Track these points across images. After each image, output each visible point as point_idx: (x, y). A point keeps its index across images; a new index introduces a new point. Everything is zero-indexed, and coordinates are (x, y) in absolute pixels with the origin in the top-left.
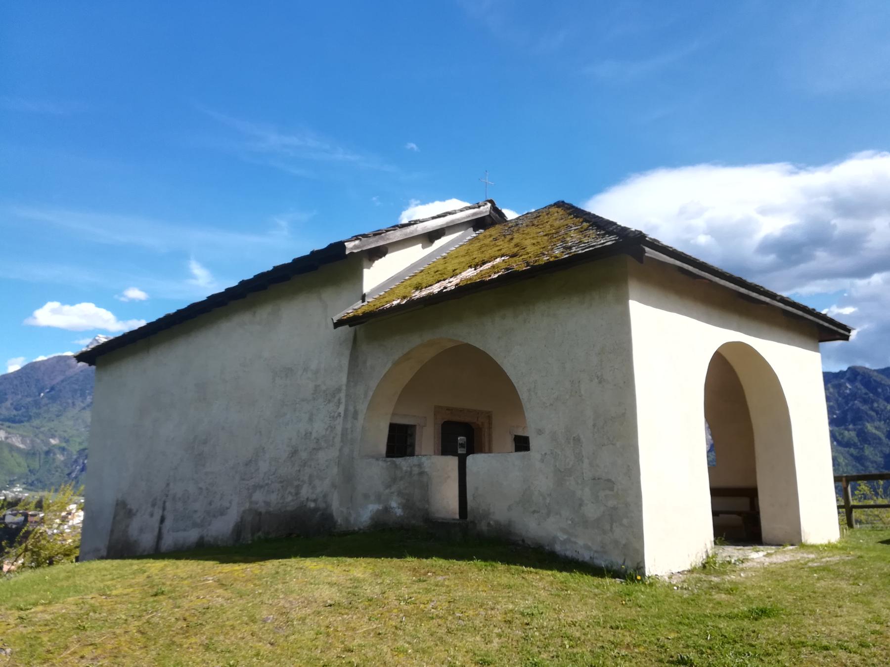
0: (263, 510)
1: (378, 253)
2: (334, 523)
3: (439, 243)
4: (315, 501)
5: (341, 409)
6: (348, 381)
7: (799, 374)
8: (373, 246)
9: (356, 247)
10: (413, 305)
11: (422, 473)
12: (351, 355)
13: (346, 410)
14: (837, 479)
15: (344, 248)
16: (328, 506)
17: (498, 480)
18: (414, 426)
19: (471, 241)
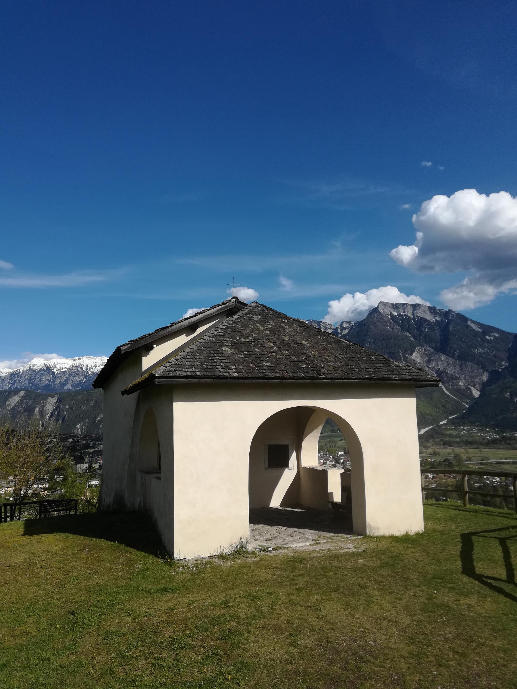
1: (148, 348)
9: (128, 348)
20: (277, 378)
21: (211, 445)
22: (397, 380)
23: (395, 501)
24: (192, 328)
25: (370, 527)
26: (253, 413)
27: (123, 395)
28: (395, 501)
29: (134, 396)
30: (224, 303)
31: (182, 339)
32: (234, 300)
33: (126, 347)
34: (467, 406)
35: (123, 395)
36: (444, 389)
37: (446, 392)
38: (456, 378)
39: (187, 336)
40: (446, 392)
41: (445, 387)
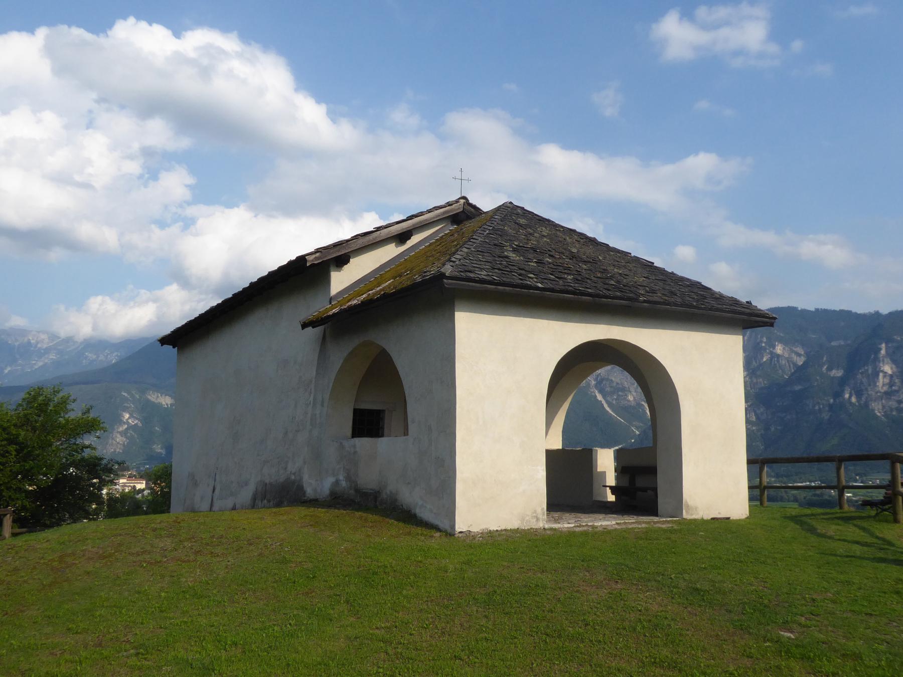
0: (267, 481)
1: (341, 261)
2: (304, 493)
3: (415, 239)
4: (294, 474)
5: (311, 399)
6: (317, 373)
7: (708, 375)
8: (334, 255)
9: (316, 258)
10: (386, 298)
11: (355, 452)
12: (321, 351)
13: (315, 399)
14: (750, 462)
15: (306, 261)
16: (301, 479)
17: (384, 460)
18: (383, 411)
19: (451, 234)
20: (589, 295)
21: (501, 378)
22: (729, 312)
23: (714, 478)
24: (402, 238)
25: (688, 506)
26: (558, 337)
27: (303, 328)
28: (714, 478)
29: (319, 330)
30: (449, 204)
31: (391, 251)
32: (462, 201)
33: (314, 256)
34: (637, 433)
35: (303, 328)
36: (606, 406)
37: (608, 409)
38: (623, 389)
39: (397, 246)
40: (608, 409)
41: (607, 402)
